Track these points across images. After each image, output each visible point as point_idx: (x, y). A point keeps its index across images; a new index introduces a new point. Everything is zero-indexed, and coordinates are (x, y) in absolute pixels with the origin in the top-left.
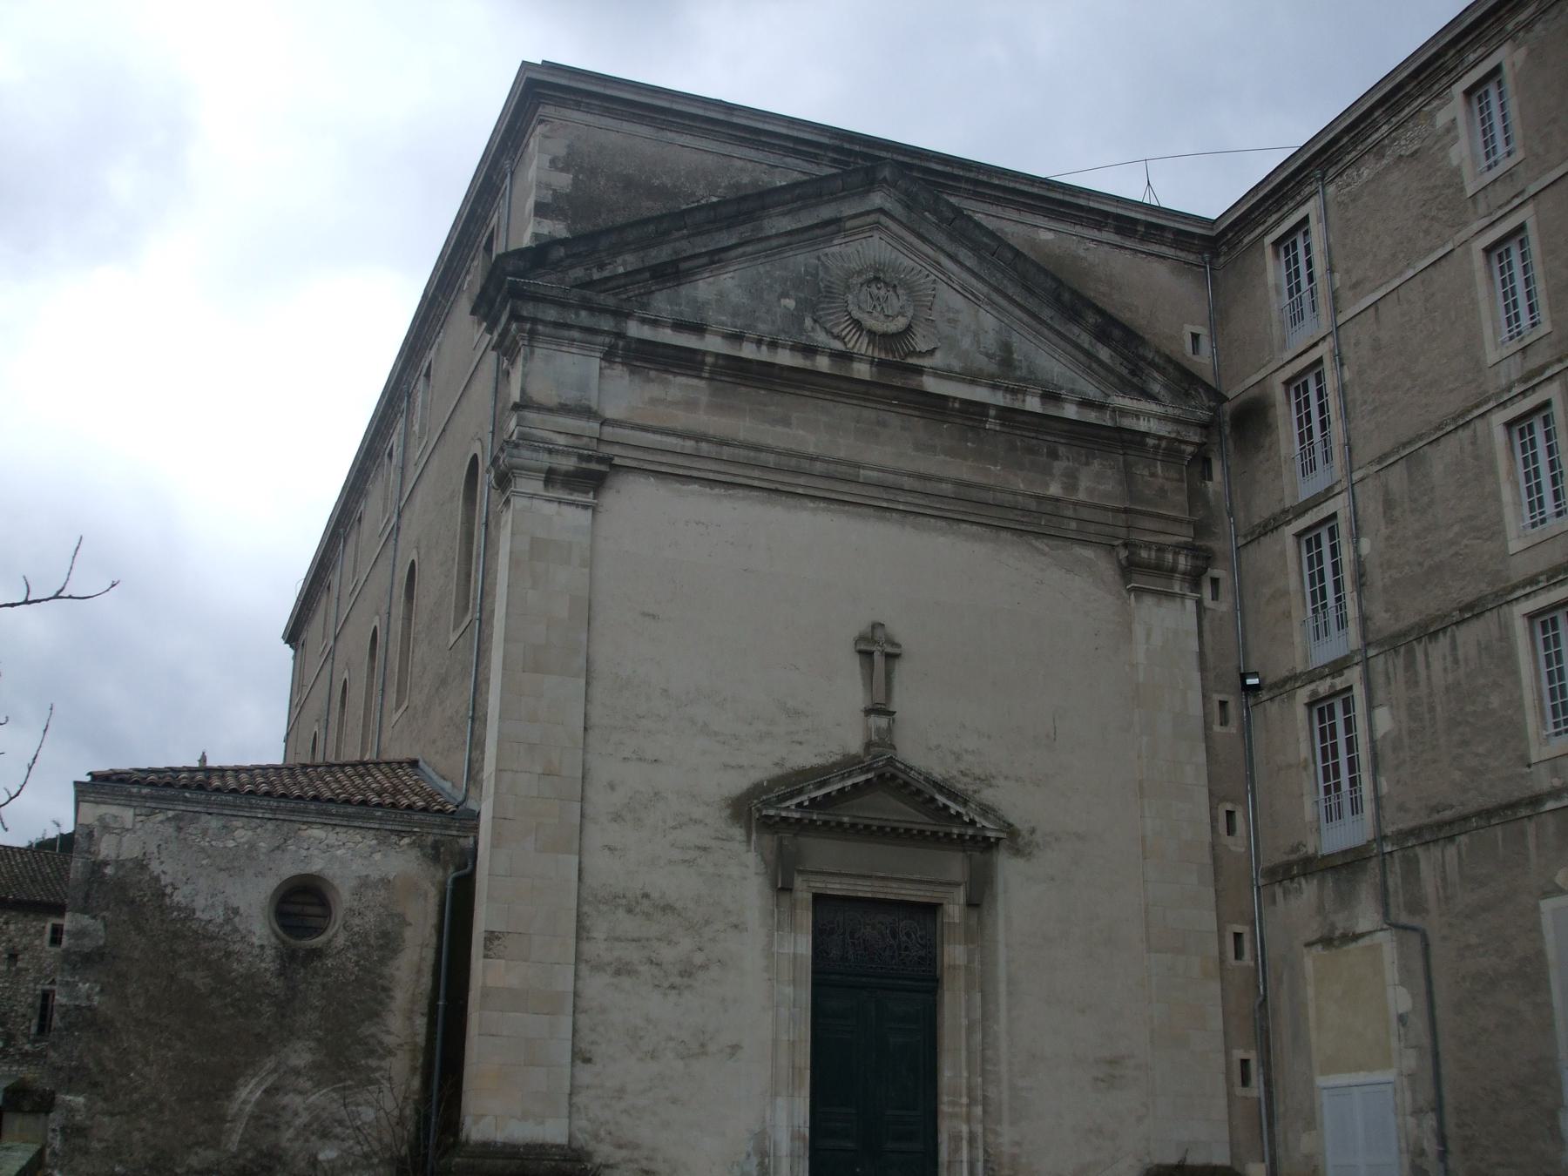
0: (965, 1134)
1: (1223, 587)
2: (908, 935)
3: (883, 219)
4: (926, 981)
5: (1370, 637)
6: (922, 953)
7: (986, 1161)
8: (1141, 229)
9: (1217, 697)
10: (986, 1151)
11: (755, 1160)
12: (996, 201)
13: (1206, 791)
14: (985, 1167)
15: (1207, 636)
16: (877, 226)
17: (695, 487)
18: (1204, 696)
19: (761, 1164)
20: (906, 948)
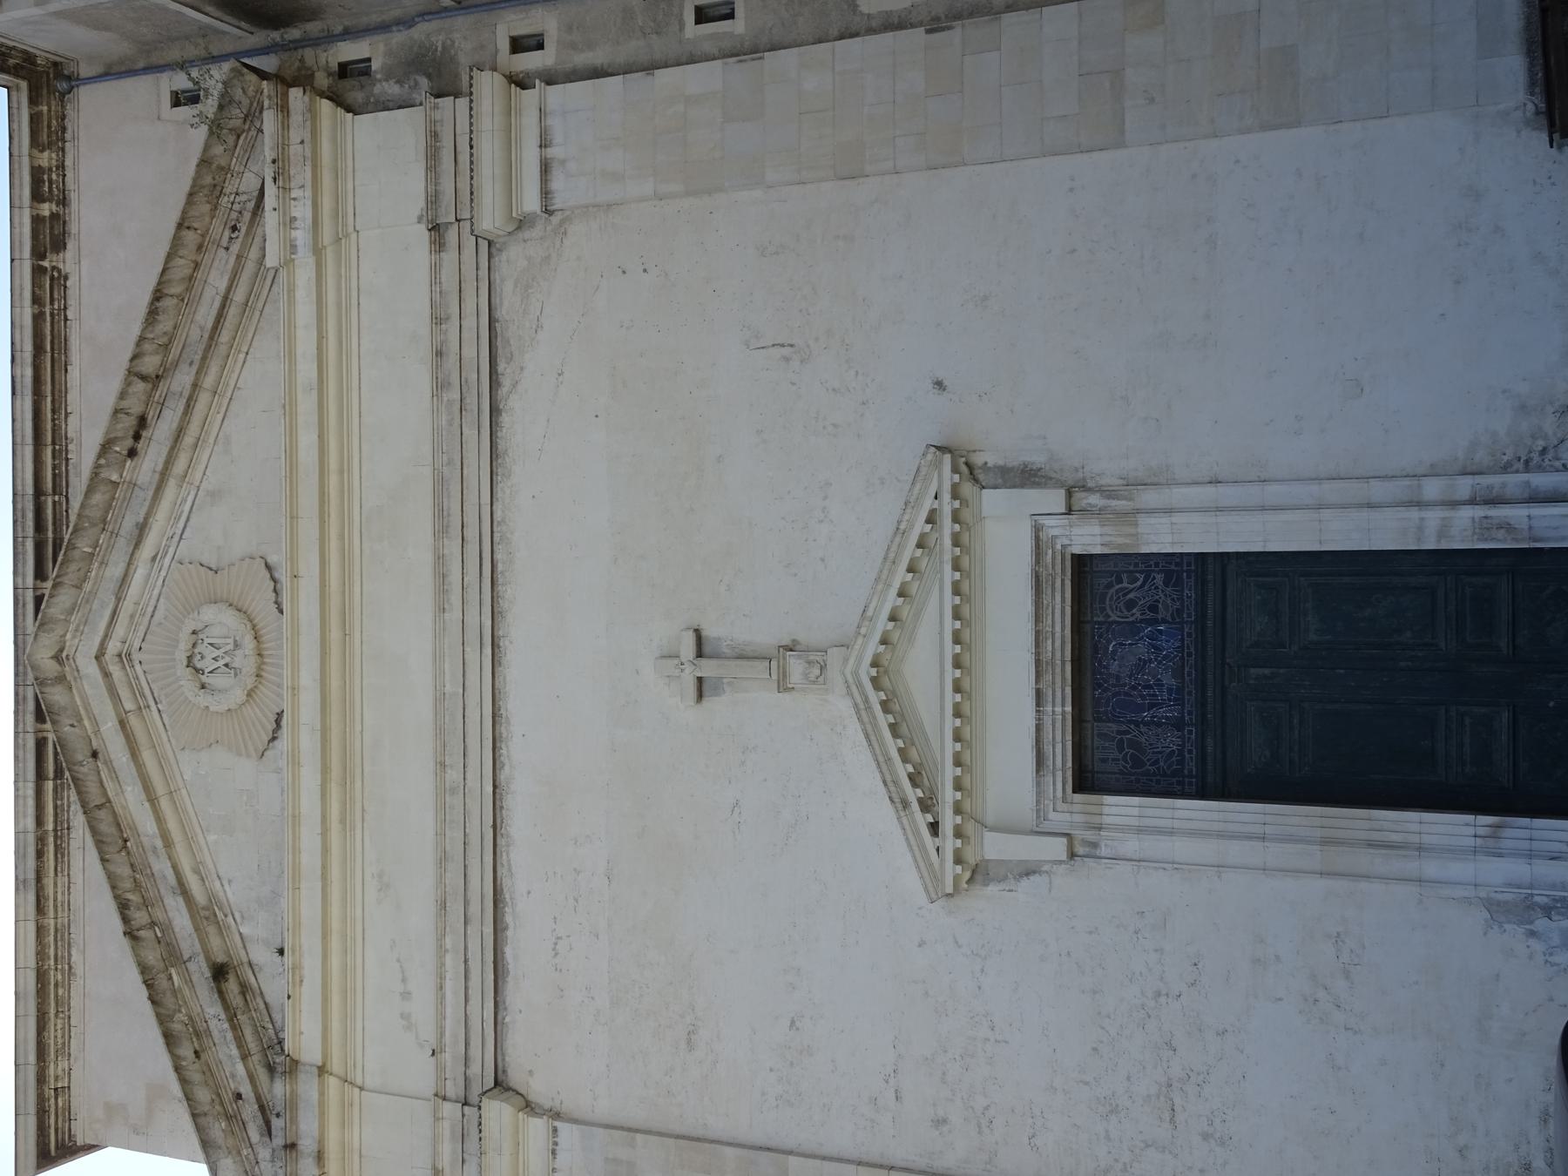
0: (1480, 512)
1: (522, 30)
2: (1131, 605)
3: (113, 647)
4: (1209, 585)
5: (87, 512)
6: (1159, 579)
7: (1527, 466)
8: (46, 209)
9: (692, 30)
10: (1506, 469)
11: (1541, 924)
12: (61, 455)
13: (837, 43)
14: (1541, 469)
15: (597, 57)
16: (124, 658)
17: (509, 952)
18: (692, 60)
19: (1547, 911)
20: (1153, 608)
